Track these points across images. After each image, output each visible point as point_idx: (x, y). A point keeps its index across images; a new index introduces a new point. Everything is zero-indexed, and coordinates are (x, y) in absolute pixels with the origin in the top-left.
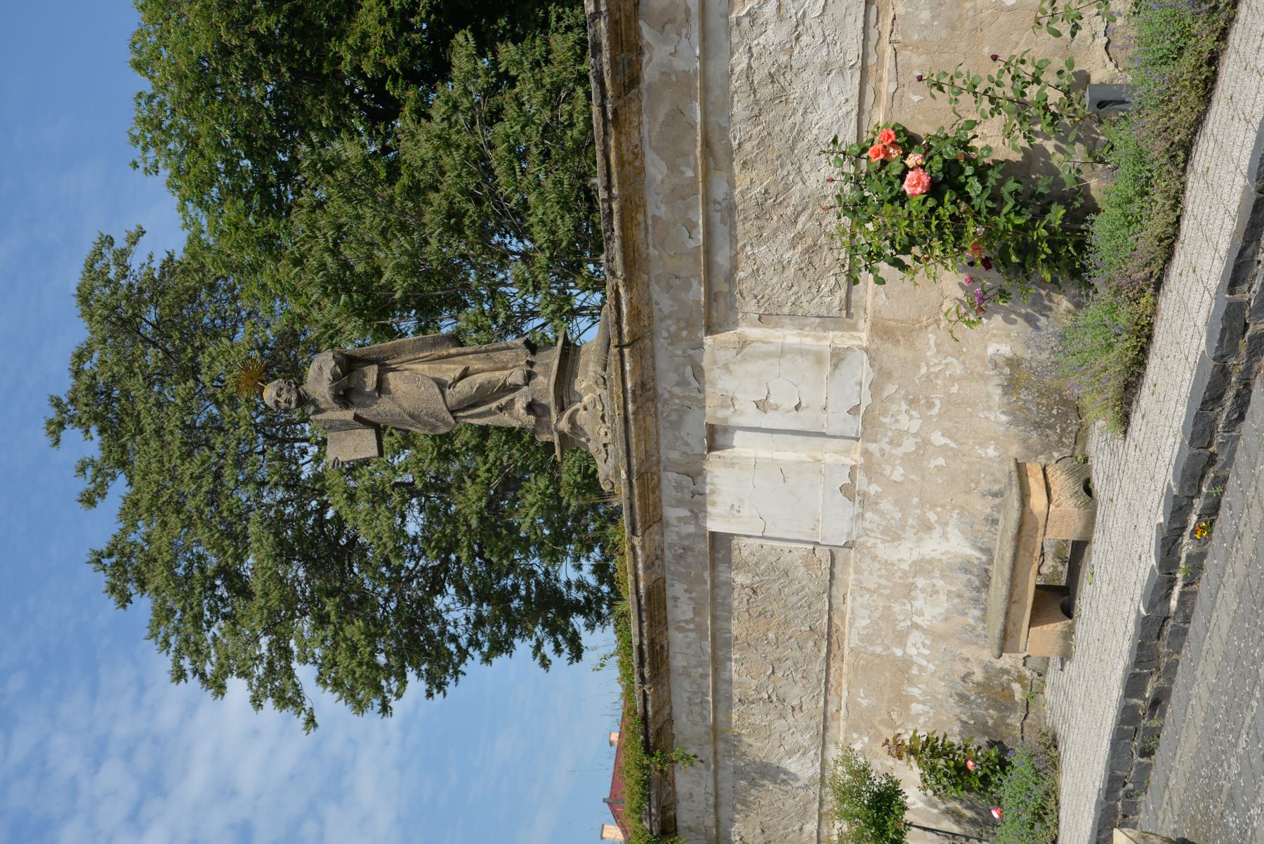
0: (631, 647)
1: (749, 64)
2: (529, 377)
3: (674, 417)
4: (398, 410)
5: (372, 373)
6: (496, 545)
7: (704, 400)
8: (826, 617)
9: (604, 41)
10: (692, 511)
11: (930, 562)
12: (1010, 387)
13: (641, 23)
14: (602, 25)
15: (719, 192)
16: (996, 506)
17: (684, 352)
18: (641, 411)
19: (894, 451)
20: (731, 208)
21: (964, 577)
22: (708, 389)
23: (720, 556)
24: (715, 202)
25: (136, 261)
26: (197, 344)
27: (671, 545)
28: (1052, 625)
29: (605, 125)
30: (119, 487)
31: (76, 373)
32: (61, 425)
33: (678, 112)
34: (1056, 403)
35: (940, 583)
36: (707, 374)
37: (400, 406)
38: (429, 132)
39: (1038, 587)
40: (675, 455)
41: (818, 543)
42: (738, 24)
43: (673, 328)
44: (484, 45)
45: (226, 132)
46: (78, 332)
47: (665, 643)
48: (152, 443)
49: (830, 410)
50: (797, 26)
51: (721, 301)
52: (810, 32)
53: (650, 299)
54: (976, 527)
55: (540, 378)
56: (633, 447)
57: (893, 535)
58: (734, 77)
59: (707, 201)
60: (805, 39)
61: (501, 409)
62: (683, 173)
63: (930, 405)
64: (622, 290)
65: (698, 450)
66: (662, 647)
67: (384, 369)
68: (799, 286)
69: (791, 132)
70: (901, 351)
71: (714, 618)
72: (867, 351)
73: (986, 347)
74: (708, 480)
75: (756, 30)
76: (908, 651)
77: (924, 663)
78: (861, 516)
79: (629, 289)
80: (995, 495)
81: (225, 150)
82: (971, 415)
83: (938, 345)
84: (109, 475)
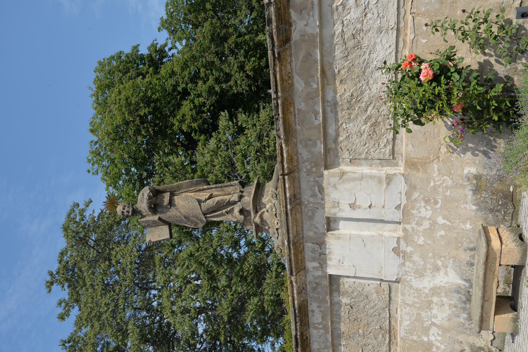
0: (291, 338)
1: (342, 29)
2: (241, 197)
3: (310, 214)
4: (179, 214)
5: (167, 197)
6: (236, 334)
7: (324, 204)
8: (388, 321)
9: (273, 17)
10: (320, 264)
11: (439, 288)
12: (477, 190)
13: (291, 10)
14: (272, 9)
15: (329, 96)
16: (472, 256)
17: (314, 179)
18: (294, 210)
19: (418, 229)
20: (335, 104)
21: (457, 296)
22: (326, 198)
23: (334, 288)
24: (328, 101)
25: (87, 214)
26: (111, 247)
27: (310, 282)
28: (506, 315)
29: (274, 60)
30: (75, 312)
31: (60, 261)
32: (52, 283)
33: (309, 55)
34: (501, 198)
35: (445, 300)
36: (325, 190)
37: (180, 212)
38: (208, 149)
39: (497, 297)
40: (311, 234)
41: (382, 280)
42: (337, 9)
43: (309, 167)
44: (232, 117)
45: (126, 156)
46: (62, 243)
47: (308, 335)
48: (90, 290)
49: (386, 207)
50: (365, 9)
51: (332, 153)
52: (371, 12)
53: (297, 152)
54: (462, 268)
55: (246, 198)
56: (290, 228)
57: (420, 274)
58: (335, 37)
59: (324, 101)
60: (369, 15)
61: (227, 213)
62: (312, 86)
63: (436, 203)
64: (283, 146)
65: (322, 231)
66: (307, 338)
67: (172, 195)
68: (369, 143)
69: (363, 63)
70: (420, 175)
71: (332, 322)
72: (403, 175)
73: (463, 170)
74: (327, 246)
75: (346, 12)
76: (430, 338)
77: (439, 345)
78: (403, 264)
79: (287, 145)
80: (471, 250)
81: (126, 163)
82: (457, 207)
83: (439, 170)
84: (71, 306)
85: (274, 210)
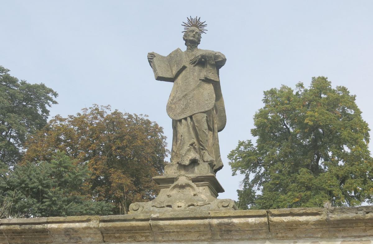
85: (199, 203)
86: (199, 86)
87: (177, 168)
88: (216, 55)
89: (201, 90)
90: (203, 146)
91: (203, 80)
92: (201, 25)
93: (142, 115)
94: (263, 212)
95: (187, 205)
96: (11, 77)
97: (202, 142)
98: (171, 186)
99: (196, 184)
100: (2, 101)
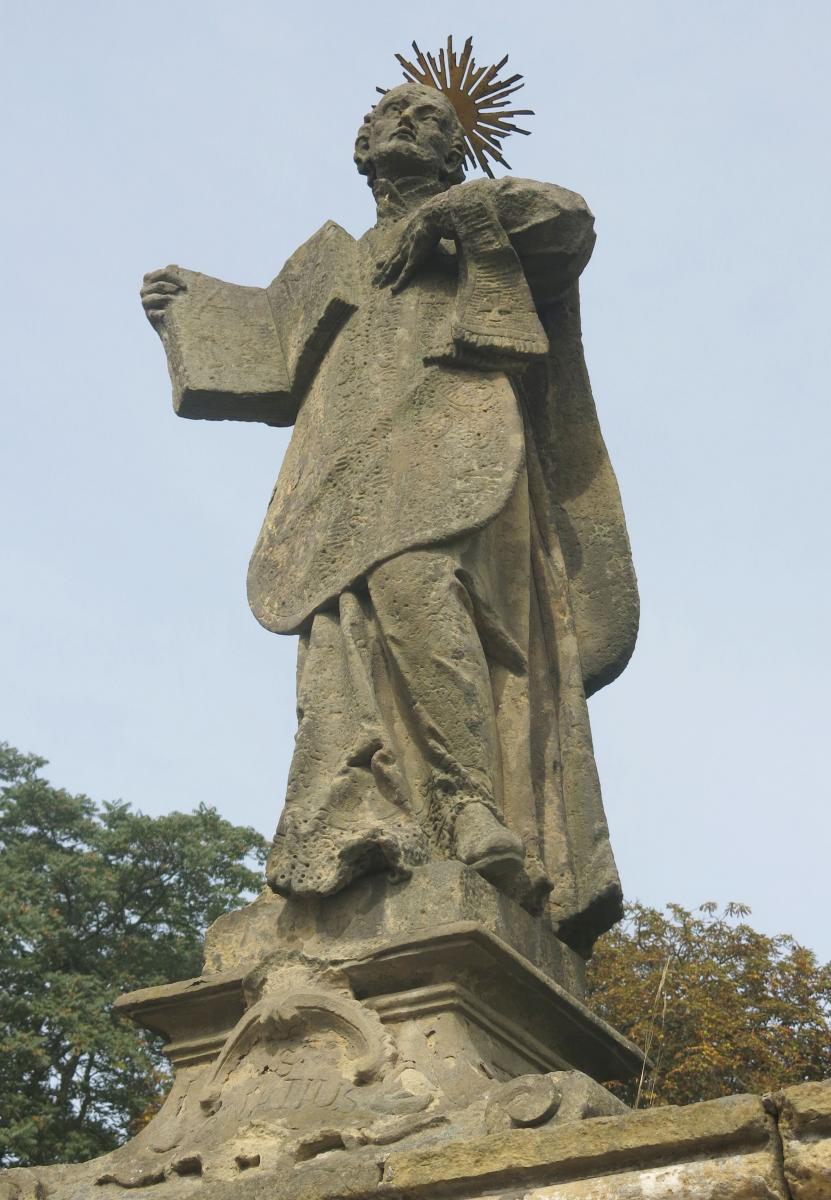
85: (381, 1126)
86: (416, 401)
87: (279, 922)
88: (511, 191)
89: (434, 421)
90: (448, 768)
91: (444, 363)
92: (484, 89)
93: (711, 907)
94: (734, 1114)
95: (293, 1147)
96: (54, 793)
97: (441, 741)
98: (222, 1043)
99: (380, 1010)
100: (13, 912)
